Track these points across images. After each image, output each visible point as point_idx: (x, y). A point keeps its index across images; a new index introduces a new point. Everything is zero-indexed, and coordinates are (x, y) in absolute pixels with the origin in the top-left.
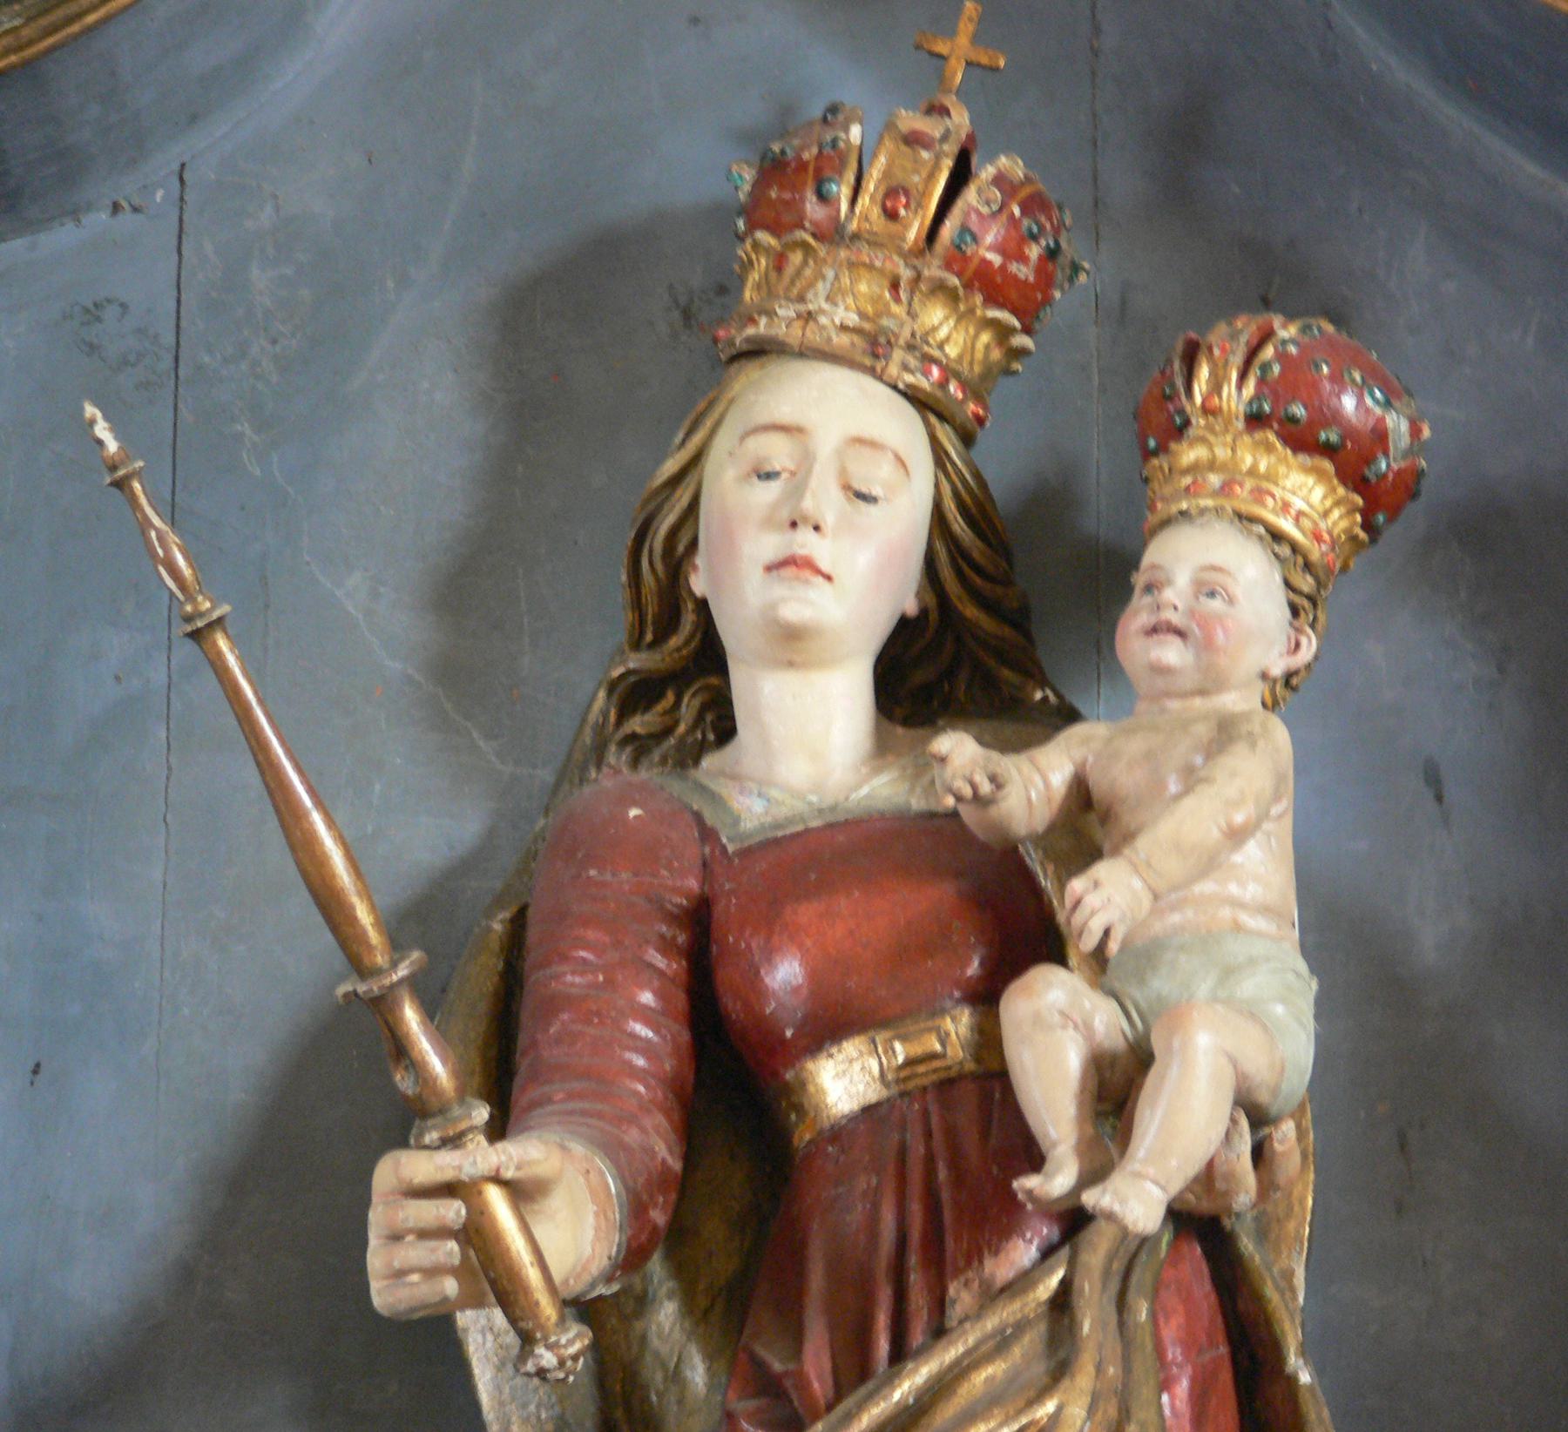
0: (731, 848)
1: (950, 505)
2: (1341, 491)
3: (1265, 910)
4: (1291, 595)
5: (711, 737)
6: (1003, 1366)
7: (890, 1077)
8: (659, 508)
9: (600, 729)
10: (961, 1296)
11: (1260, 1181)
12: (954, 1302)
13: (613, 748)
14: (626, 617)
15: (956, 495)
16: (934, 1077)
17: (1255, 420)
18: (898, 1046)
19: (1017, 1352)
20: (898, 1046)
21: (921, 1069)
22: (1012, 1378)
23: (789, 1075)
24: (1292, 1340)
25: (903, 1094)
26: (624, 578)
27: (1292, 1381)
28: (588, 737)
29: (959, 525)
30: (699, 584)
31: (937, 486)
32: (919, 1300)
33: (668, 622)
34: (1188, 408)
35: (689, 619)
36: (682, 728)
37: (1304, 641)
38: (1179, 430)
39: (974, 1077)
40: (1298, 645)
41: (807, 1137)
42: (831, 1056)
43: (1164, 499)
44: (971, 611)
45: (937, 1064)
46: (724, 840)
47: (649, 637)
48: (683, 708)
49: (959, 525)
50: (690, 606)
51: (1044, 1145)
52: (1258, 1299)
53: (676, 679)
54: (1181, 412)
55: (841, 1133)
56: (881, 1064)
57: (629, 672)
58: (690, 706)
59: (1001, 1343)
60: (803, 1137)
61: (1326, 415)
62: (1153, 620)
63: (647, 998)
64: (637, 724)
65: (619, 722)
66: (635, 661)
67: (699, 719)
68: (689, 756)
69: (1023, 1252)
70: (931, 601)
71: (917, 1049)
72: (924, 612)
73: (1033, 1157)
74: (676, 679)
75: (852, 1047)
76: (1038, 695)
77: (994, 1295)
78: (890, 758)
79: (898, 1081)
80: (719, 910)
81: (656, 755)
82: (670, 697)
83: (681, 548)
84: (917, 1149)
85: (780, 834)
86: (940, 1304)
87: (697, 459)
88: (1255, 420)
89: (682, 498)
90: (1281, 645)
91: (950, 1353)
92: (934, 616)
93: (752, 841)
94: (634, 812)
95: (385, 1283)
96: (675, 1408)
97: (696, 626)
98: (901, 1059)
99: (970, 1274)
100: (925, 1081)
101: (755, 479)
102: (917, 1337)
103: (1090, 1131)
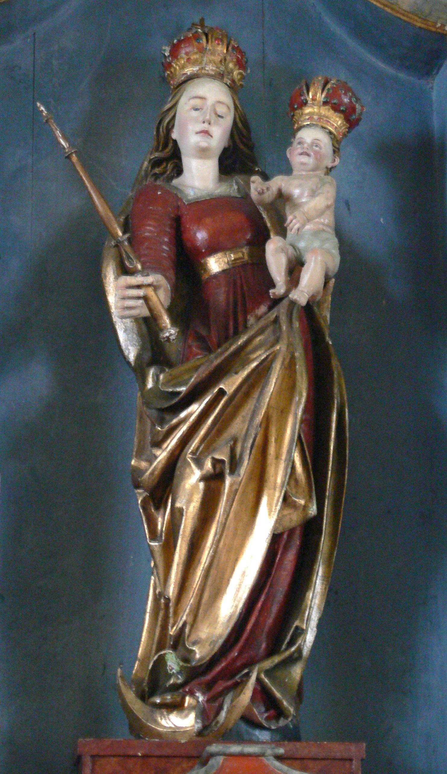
0: (186, 203)
1: (238, 120)
2: (345, 123)
3: (328, 226)
4: (334, 148)
5: (176, 175)
6: (264, 337)
7: (230, 263)
8: (165, 116)
9: (146, 171)
10: (251, 320)
11: (324, 293)
12: (249, 320)
13: (150, 176)
14: (155, 144)
15: (239, 117)
16: (241, 264)
17: (325, 103)
18: (232, 255)
19: (266, 333)
20: (232, 255)
21: (238, 261)
22: (265, 340)
23: (202, 261)
24: (327, 332)
25: (234, 267)
26: (155, 133)
27: (328, 343)
28: (143, 173)
29: (240, 125)
30: (174, 135)
31: (235, 115)
32: (241, 319)
33: (166, 145)
34: (308, 99)
35: (171, 145)
36: (168, 172)
37: (336, 159)
38: (305, 104)
39: (252, 264)
40: (335, 160)
41: (207, 277)
42: (214, 257)
43: (301, 121)
44: (242, 147)
45: (242, 260)
46: (184, 201)
47: (160, 149)
48: (168, 168)
49: (240, 125)
50: (171, 141)
51: (275, 281)
52: (319, 323)
53: (166, 160)
54: (306, 100)
55: (216, 276)
56: (228, 260)
57: (156, 157)
58: (170, 166)
59: (261, 331)
60: (206, 277)
61: (341, 103)
62: (302, 151)
63: (166, 240)
64: (157, 170)
65: (151, 171)
66: (157, 154)
67: (172, 170)
68: (170, 179)
69: (263, 309)
70: (231, 144)
71: (237, 257)
72: (229, 146)
73: (272, 285)
74: (166, 160)
75: (219, 255)
76: (257, 169)
77: (259, 318)
78: (223, 183)
79: (232, 264)
80: (183, 219)
81: (162, 178)
82: (165, 164)
83: (170, 127)
84: (239, 281)
85: (199, 200)
86: (246, 321)
87: (175, 104)
88: (325, 103)
89: (171, 114)
90: (330, 161)
91: (251, 333)
92: (232, 147)
93: (192, 202)
94: (159, 193)
95: (120, 310)
96: (297, 354)
97: (172, 147)
98: (233, 259)
99: (252, 313)
100: (239, 265)
101: (193, 110)
102: (241, 329)
103: (289, 278)
